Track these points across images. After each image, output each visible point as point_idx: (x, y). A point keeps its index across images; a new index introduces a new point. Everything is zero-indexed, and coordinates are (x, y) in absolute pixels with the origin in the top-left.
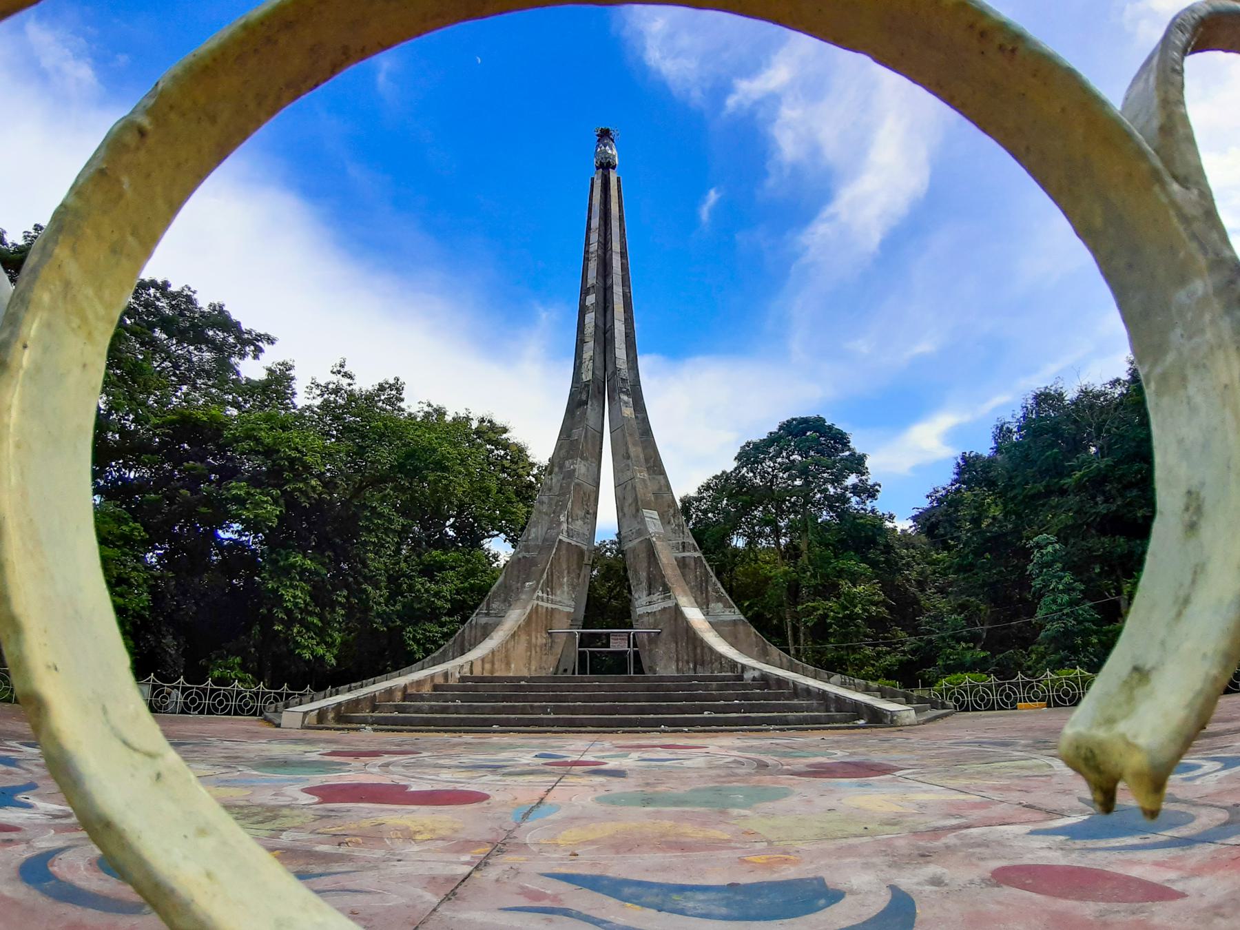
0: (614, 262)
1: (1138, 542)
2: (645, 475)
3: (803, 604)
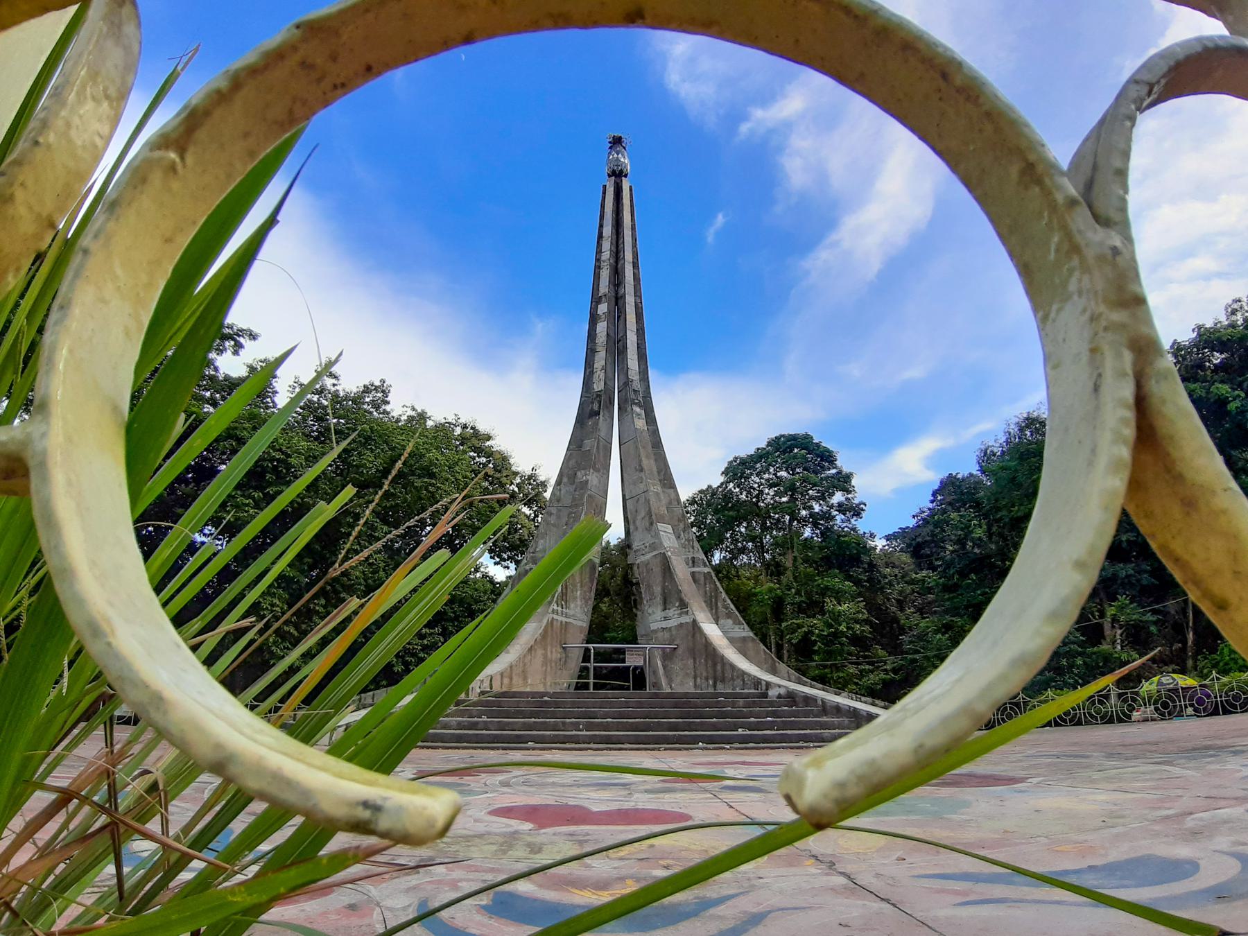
1: (1122, 565)
2: (658, 488)
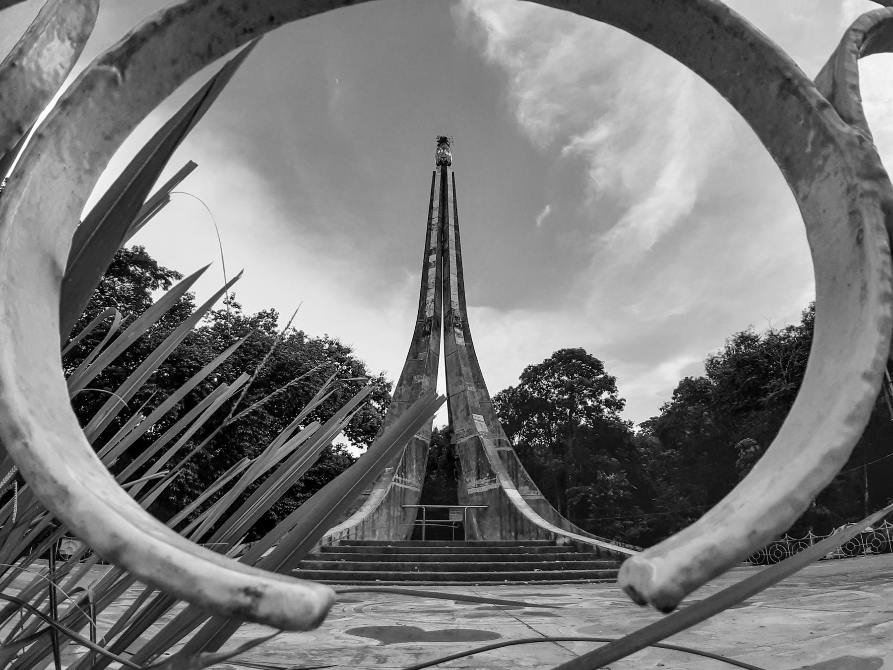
0: (450, 232)
3: (569, 488)
